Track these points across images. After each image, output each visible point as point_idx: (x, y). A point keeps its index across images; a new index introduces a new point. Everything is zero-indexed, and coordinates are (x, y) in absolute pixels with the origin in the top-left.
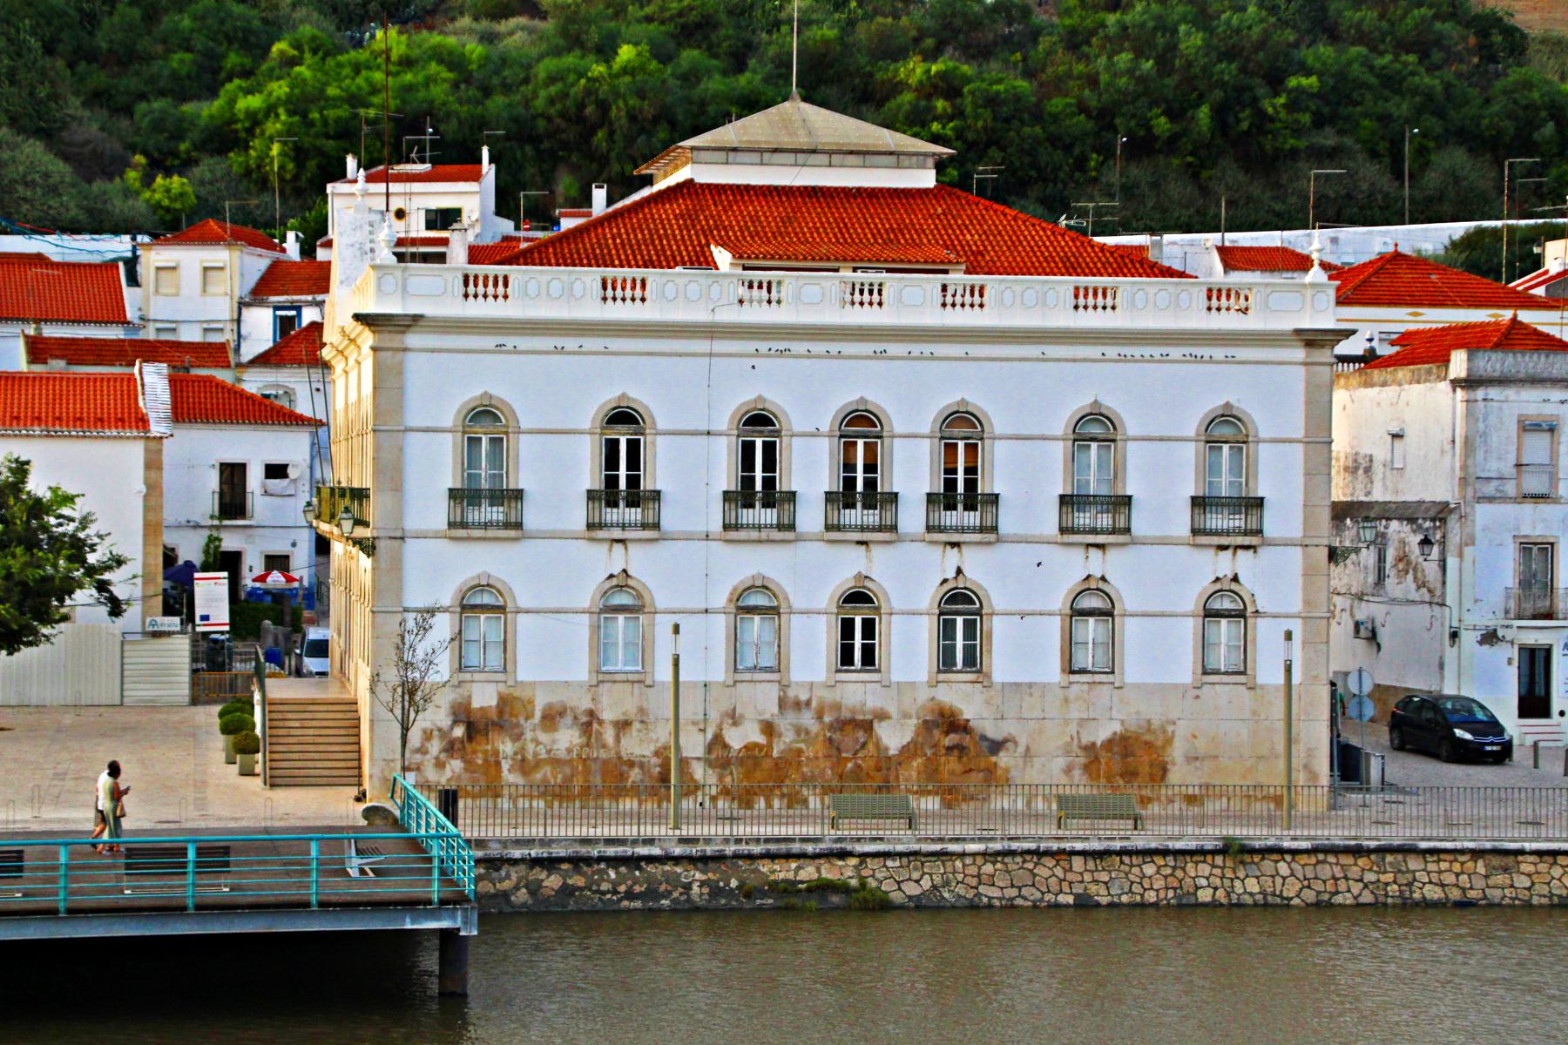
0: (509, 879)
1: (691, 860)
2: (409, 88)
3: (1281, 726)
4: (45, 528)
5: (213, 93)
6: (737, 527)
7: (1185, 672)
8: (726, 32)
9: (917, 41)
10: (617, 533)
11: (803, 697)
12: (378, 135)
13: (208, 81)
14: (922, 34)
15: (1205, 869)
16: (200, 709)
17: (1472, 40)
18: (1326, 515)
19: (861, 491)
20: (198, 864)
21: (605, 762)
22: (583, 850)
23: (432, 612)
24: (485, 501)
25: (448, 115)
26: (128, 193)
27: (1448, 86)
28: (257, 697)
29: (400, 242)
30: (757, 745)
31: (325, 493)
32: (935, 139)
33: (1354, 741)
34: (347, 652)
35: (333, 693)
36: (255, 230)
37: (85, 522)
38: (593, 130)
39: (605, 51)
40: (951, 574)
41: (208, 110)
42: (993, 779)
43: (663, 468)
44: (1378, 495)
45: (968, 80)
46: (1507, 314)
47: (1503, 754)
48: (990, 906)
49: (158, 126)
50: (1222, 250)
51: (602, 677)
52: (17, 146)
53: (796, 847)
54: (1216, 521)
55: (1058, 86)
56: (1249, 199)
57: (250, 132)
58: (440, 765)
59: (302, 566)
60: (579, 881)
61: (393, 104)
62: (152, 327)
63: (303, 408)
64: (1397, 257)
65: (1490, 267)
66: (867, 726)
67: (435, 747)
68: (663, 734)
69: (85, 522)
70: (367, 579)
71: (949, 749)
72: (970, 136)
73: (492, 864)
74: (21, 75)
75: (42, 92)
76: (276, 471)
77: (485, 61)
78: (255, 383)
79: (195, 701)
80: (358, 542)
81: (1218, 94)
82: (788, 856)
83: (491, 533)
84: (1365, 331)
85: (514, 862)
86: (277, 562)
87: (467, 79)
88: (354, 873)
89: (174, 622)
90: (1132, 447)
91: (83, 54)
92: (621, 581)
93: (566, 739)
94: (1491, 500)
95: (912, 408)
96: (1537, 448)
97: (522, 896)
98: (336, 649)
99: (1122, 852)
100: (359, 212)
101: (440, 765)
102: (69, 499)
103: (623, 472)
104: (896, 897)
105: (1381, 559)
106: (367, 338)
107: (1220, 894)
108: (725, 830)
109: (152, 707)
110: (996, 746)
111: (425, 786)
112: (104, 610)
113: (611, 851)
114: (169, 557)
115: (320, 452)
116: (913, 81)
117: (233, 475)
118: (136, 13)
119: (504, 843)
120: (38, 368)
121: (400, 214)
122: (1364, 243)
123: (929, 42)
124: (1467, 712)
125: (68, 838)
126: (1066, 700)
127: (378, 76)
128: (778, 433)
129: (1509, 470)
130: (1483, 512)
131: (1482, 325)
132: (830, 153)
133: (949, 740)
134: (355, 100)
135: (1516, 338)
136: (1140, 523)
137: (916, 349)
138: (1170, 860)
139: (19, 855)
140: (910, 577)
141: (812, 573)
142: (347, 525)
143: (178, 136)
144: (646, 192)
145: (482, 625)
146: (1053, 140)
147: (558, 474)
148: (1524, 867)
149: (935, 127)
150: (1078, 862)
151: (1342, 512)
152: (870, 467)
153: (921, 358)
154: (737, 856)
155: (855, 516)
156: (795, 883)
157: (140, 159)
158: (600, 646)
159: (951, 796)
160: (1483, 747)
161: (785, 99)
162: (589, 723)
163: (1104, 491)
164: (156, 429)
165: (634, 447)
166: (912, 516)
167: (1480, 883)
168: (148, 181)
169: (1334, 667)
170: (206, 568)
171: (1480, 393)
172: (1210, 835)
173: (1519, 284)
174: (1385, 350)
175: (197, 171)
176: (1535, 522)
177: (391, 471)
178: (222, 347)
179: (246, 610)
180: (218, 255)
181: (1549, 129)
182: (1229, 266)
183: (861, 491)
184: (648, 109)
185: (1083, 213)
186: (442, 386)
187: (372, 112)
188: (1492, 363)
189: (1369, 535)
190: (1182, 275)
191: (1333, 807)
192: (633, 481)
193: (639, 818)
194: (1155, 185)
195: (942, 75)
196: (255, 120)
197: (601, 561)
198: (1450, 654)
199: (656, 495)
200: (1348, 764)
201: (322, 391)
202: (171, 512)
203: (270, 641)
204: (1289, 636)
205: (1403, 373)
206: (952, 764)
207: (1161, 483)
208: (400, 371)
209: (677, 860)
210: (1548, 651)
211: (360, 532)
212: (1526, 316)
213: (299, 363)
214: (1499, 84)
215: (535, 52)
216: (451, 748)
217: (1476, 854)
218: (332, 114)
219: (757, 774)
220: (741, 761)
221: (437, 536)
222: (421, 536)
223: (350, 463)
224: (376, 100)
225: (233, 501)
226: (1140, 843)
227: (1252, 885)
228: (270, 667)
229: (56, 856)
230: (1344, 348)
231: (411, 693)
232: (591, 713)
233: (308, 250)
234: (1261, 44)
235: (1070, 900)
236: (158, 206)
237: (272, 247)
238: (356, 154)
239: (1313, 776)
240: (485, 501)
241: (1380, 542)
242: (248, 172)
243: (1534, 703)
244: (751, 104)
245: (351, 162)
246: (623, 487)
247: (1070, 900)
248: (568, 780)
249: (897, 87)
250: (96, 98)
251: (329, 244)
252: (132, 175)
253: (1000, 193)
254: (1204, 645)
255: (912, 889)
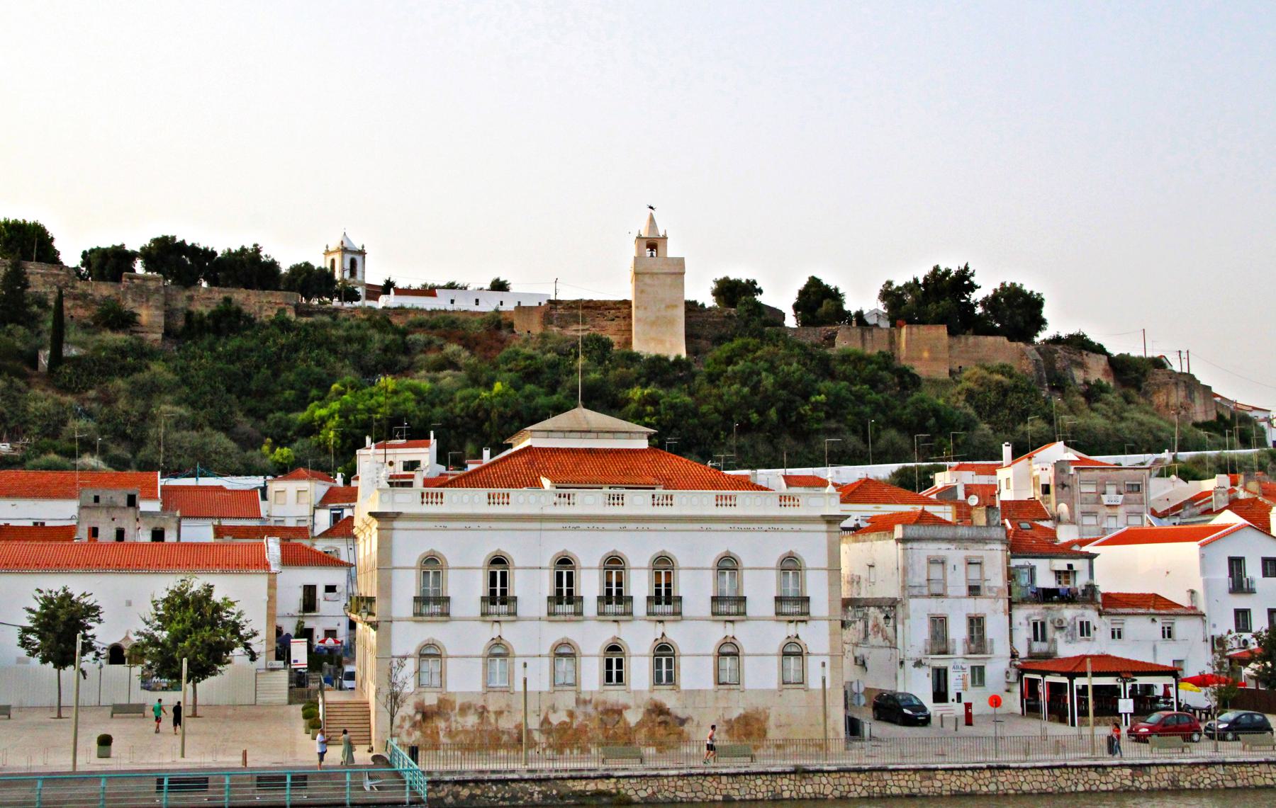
0: (444, 791)
1: (533, 780)
2: (396, 404)
3: (821, 709)
4: (220, 618)
5: (304, 409)
6: (555, 614)
7: (773, 683)
8: (548, 374)
9: (637, 379)
10: (496, 618)
11: (588, 698)
12: (381, 426)
13: (302, 402)
14: (640, 376)
15: (786, 781)
16: (293, 706)
17: (896, 380)
18: (839, 605)
19: (614, 596)
20: (292, 785)
21: (491, 732)
22: (480, 776)
23: (405, 657)
24: (432, 603)
25: (415, 416)
26: (263, 456)
27: (886, 401)
28: (320, 700)
29: (391, 477)
30: (565, 722)
31: (354, 600)
32: (647, 425)
33: (856, 716)
34: (364, 678)
35: (357, 698)
36: (322, 471)
37: (240, 615)
38: (483, 423)
39: (489, 386)
40: (659, 636)
41: (301, 416)
42: (682, 738)
43: (517, 586)
44: (863, 595)
45: (662, 397)
46: (919, 508)
47: (926, 721)
48: (681, 802)
49: (278, 424)
50: (785, 477)
51: (489, 689)
52: (212, 435)
53: (585, 774)
54: (787, 608)
55: (705, 400)
56: (797, 453)
57: (320, 426)
58: (409, 734)
59: (343, 634)
60: (478, 792)
61: (388, 412)
62: (272, 520)
63: (344, 558)
64: (868, 480)
65: (911, 483)
66: (620, 712)
67: (407, 725)
68: (519, 718)
69: (240, 615)
70: (374, 642)
71: (660, 723)
72: (664, 423)
73: (435, 783)
74: (216, 402)
75: (225, 410)
76: (330, 589)
77: (431, 391)
78: (321, 546)
79: (290, 703)
80: (370, 623)
81: (780, 404)
82: (582, 778)
83: (435, 618)
84: (855, 516)
85: (446, 782)
86: (330, 633)
87: (424, 399)
88: (367, 789)
89: (280, 664)
90: (746, 573)
91: (244, 393)
92: (498, 642)
93: (471, 720)
94: (916, 597)
95: (638, 554)
96: (936, 572)
97: (450, 799)
98: (358, 676)
99: (746, 774)
100: (370, 459)
101: (409, 734)
102: (232, 604)
103: (498, 587)
104: (635, 798)
105: (866, 626)
106: (375, 524)
107: (794, 794)
108: (549, 765)
109: (270, 705)
110: (683, 722)
111: (403, 745)
112: (247, 658)
113: (494, 777)
114: (279, 631)
115: (352, 579)
116: (636, 398)
117: (310, 591)
118: (269, 372)
119: (441, 773)
120: (220, 541)
121: (391, 464)
122: (852, 474)
123: (643, 380)
124: (909, 700)
125: (229, 771)
126: (717, 698)
127: (382, 399)
128: (574, 568)
129: (924, 582)
130: (913, 603)
131: (908, 513)
132: (597, 432)
133: (662, 718)
134: (370, 410)
135: (924, 518)
136: (751, 610)
137: (640, 526)
138: (769, 777)
139: (206, 780)
140: (638, 638)
141: (592, 636)
142: (364, 615)
143: (287, 429)
144: (509, 452)
145: (431, 665)
146: (704, 426)
147: (467, 589)
148: (939, 777)
149: (647, 419)
150: (724, 779)
151: (847, 603)
152: (619, 584)
153: (643, 530)
154: (556, 778)
155: (612, 608)
156: (584, 792)
157: (269, 440)
158: (487, 675)
159: (661, 746)
160: (918, 719)
161: (575, 407)
162: (483, 712)
163: (733, 594)
164: (274, 569)
165: (504, 575)
166: (640, 607)
167: (917, 785)
168: (272, 451)
169: (846, 679)
170: (297, 636)
171: (909, 545)
172: (788, 764)
173: (924, 493)
174: (864, 525)
175: (296, 445)
176: (937, 607)
177: (386, 587)
178: (305, 529)
179: (316, 658)
180: (304, 485)
181: (932, 421)
182: (788, 485)
183: (614, 596)
184: (509, 412)
185: (718, 460)
186: (411, 546)
187: (379, 416)
188: (914, 531)
189: (860, 614)
190: (767, 489)
191: (847, 749)
192: (504, 592)
193: (507, 759)
194: (752, 446)
195: (650, 395)
196: (323, 420)
197: (487, 632)
198: (900, 672)
199: (515, 599)
200: (854, 728)
201: (353, 549)
202: (281, 609)
203: (327, 672)
204: (824, 664)
205: (873, 536)
206: (661, 731)
207: (760, 589)
208: (390, 539)
209: (526, 781)
210: (946, 670)
211: (371, 618)
212: (929, 508)
213: (343, 536)
214: (910, 400)
215: (456, 385)
216: (415, 725)
217: (916, 771)
218: (359, 417)
219: (565, 737)
220: (557, 730)
221: (408, 620)
222: (400, 620)
223: (366, 585)
224: (381, 410)
225: (309, 602)
226: (754, 768)
227: (809, 789)
228: (327, 686)
229: (223, 780)
230: (845, 524)
231: (395, 699)
232: (484, 707)
233: (347, 481)
234: (800, 381)
235: (721, 798)
236: (276, 462)
237: (330, 480)
238: (371, 435)
239: (838, 734)
240: (432, 603)
241: (865, 618)
242: (319, 445)
243: (940, 695)
244: (559, 409)
245: (368, 439)
246: (498, 595)
247: (721, 798)
248: (473, 741)
249: (628, 401)
250: (250, 412)
251: (357, 479)
252: (265, 448)
253: (679, 450)
254: (783, 668)
255: (643, 794)
